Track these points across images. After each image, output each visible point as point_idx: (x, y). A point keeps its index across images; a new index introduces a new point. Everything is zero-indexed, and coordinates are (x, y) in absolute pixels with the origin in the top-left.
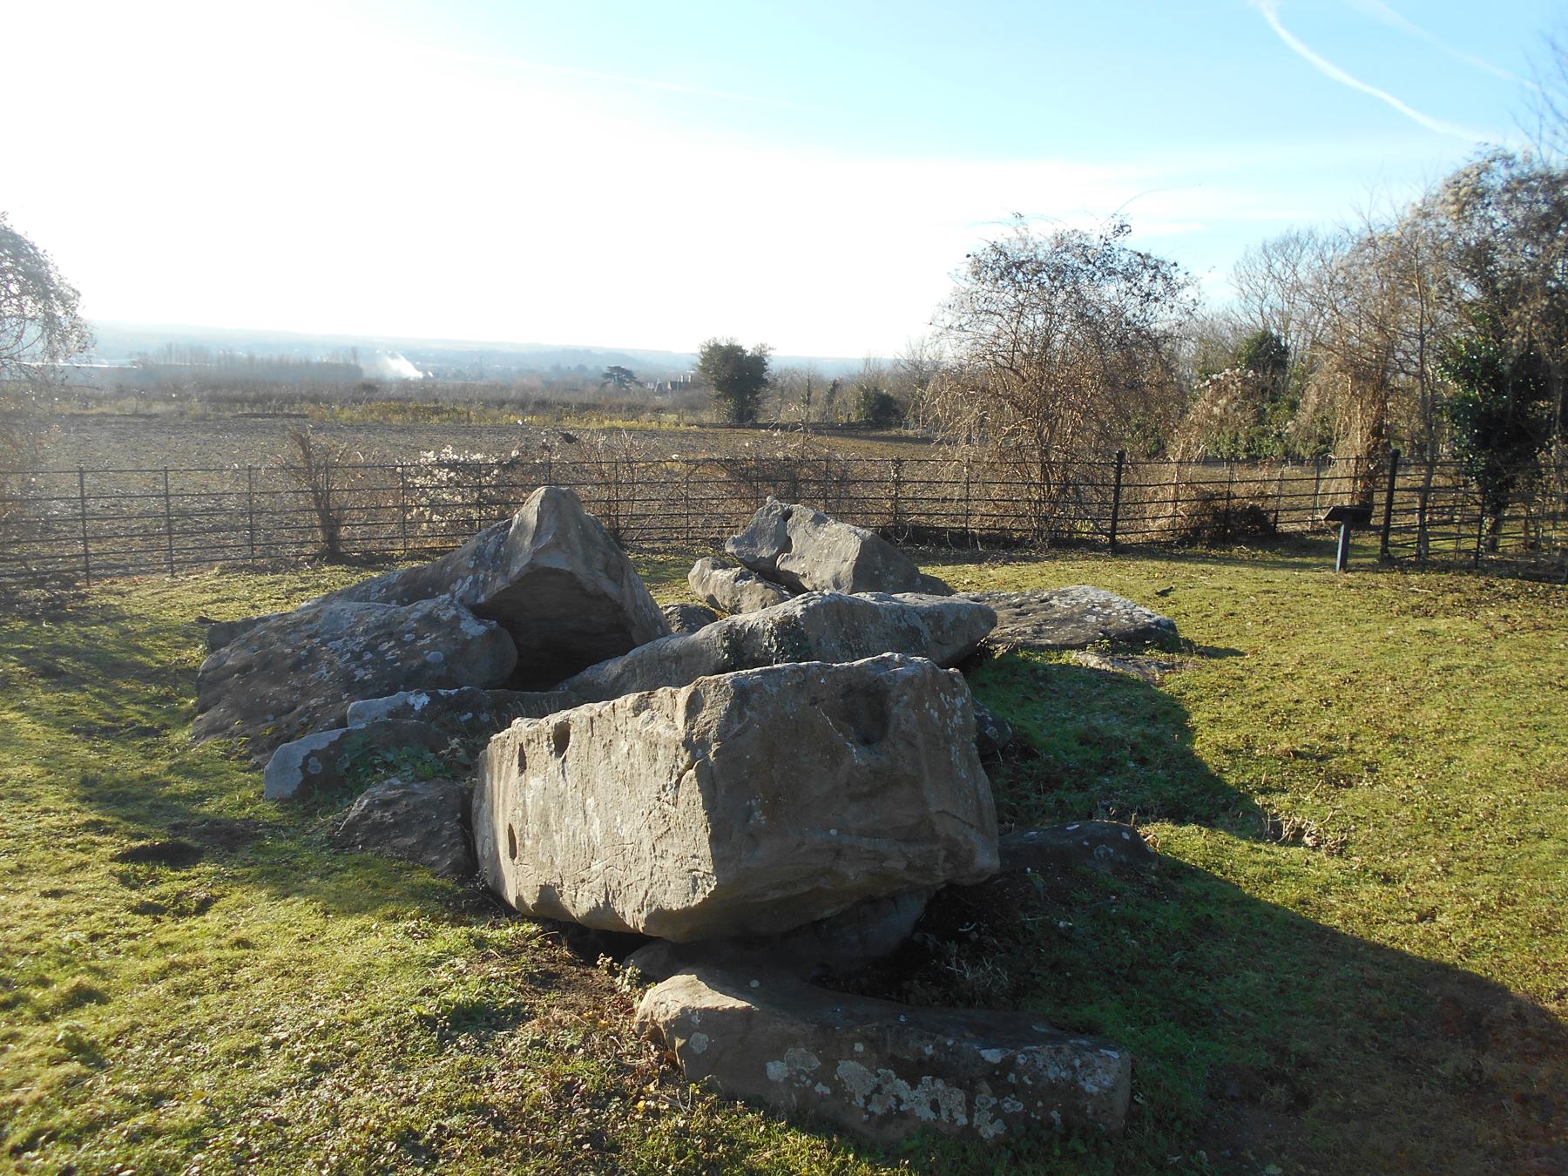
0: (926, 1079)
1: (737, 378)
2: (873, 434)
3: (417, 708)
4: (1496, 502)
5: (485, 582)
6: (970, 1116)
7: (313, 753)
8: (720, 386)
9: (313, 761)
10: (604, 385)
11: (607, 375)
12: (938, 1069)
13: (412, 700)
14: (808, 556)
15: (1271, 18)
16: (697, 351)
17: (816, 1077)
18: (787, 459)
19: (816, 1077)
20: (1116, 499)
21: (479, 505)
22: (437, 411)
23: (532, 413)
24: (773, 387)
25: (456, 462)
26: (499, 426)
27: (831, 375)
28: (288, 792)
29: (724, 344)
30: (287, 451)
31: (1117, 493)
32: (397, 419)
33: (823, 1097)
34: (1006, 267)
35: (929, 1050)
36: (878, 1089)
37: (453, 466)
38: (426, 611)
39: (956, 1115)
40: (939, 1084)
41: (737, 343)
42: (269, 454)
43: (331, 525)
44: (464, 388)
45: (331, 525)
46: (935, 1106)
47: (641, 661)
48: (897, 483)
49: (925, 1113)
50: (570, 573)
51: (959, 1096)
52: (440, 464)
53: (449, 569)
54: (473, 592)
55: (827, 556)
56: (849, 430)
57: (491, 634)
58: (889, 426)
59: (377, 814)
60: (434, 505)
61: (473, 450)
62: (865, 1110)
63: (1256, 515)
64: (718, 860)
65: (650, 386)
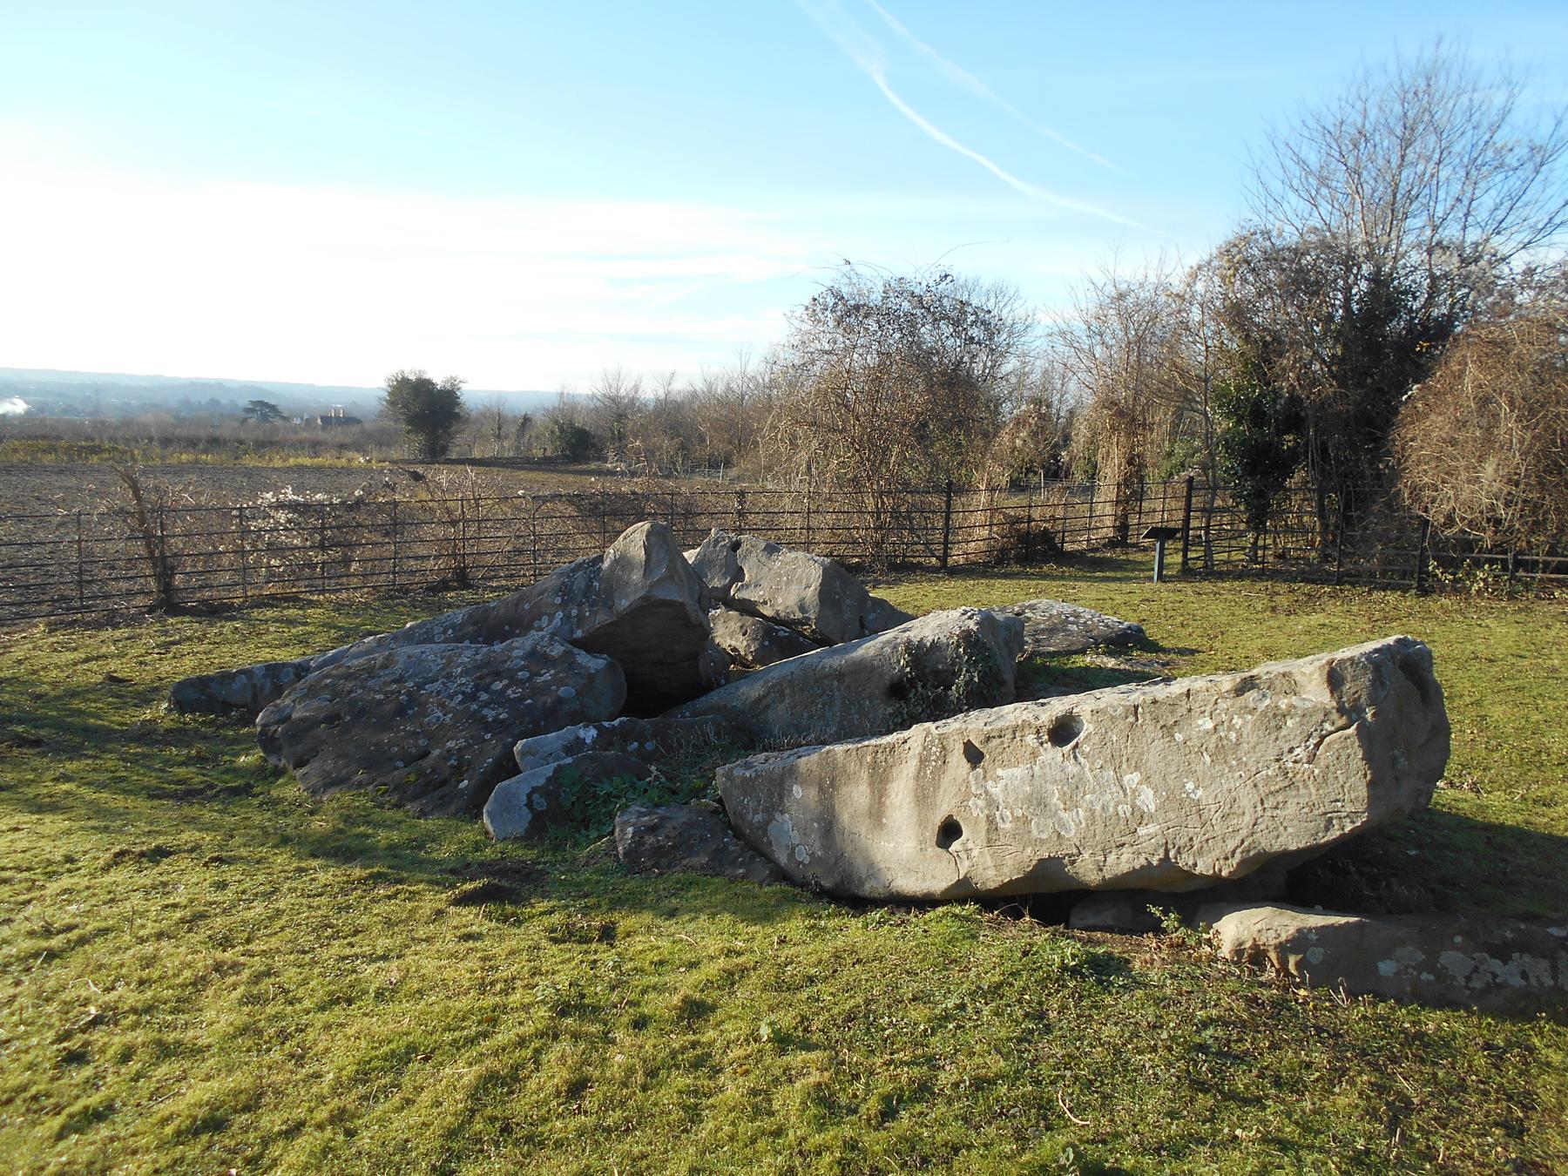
0: (1516, 955)
1: (428, 411)
2: (572, 468)
3: (588, 741)
4: (1257, 523)
5: (580, 617)
6: (1555, 978)
7: (534, 790)
8: (409, 422)
9: (536, 797)
10: (245, 420)
11: (248, 410)
12: (1523, 946)
13: (582, 733)
14: (764, 584)
15: (880, 81)
16: (384, 385)
17: (1421, 968)
18: (634, 493)
19: (1421, 968)
20: (947, 524)
21: (322, 547)
22: (95, 450)
23: (206, 451)
24: (467, 421)
25: (298, 504)
26: (170, 466)
27: (520, 407)
28: (520, 830)
29: (413, 377)
30: (121, 495)
31: (948, 519)
32: (48, 459)
33: (1428, 983)
34: (849, 311)
35: (1509, 934)
36: (1476, 970)
37: (293, 507)
38: (528, 648)
39: (1543, 979)
40: (1527, 958)
41: (427, 376)
42: (103, 498)
43: (165, 569)
44: (127, 423)
45: (165, 569)
46: (1524, 976)
47: (791, 681)
48: (741, 513)
49: (1517, 981)
50: (682, 604)
51: (1544, 964)
52: (280, 506)
53: (527, 606)
54: (567, 627)
55: (788, 583)
56: (546, 464)
57: (610, 666)
58: (587, 460)
59: (650, 840)
60: (274, 549)
61: (315, 490)
62: (1467, 987)
63: (1047, 537)
64: (1373, 800)
65: (297, 421)
